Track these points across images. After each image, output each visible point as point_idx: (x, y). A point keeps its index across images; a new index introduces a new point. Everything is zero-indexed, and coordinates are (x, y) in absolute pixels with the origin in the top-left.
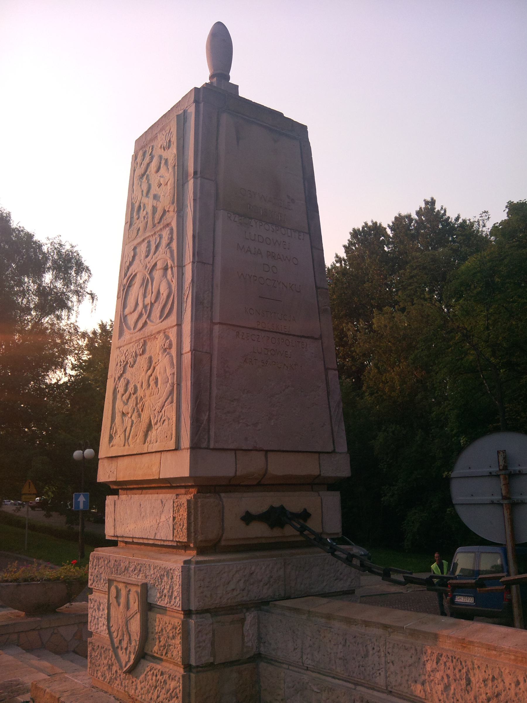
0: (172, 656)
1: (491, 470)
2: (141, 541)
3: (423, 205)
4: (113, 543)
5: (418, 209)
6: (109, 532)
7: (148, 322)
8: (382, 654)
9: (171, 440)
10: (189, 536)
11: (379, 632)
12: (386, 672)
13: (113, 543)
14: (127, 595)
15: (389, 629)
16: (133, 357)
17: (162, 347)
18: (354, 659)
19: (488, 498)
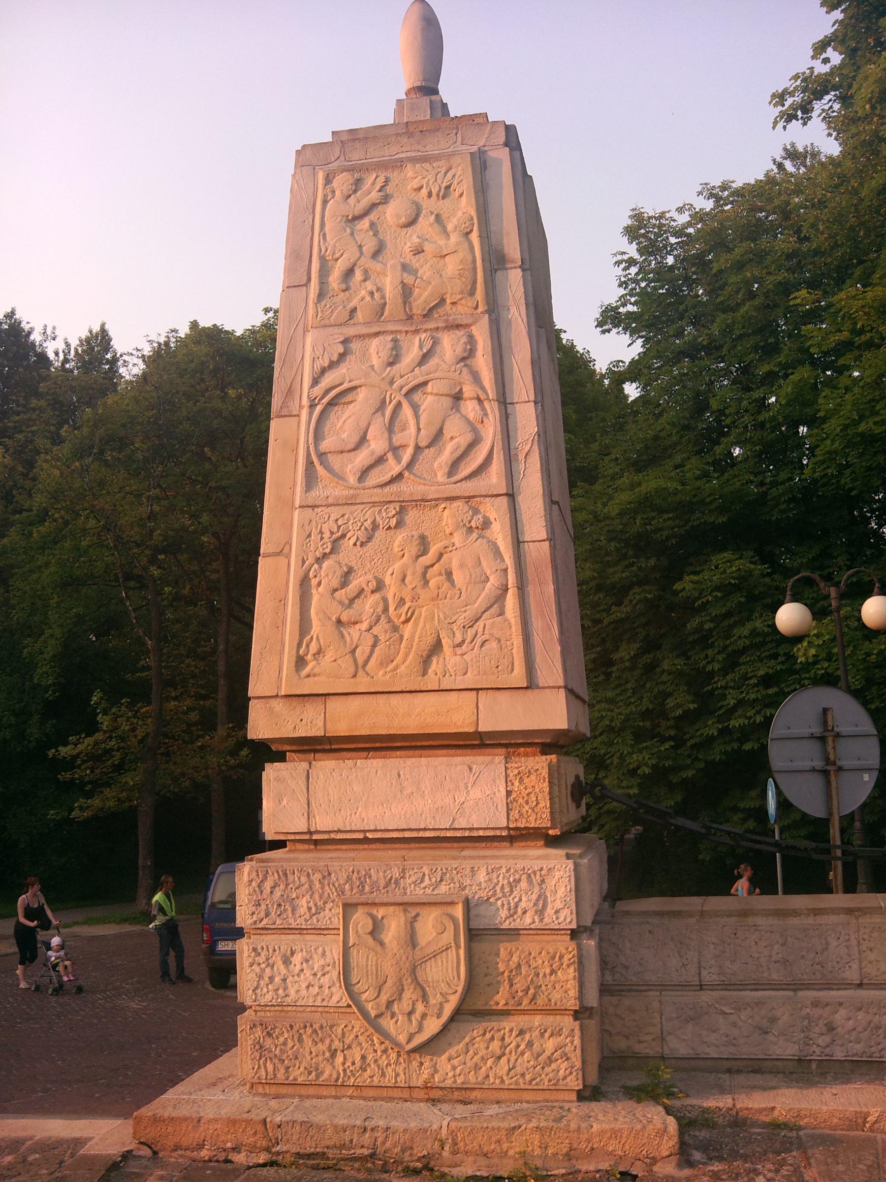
0: (550, 1000)
1: (810, 731)
2: (395, 835)
3: (184, 331)
4: (279, 845)
5: (9, 311)
6: (270, 829)
7: (406, 474)
8: (854, 943)
9: (512, 670)
10: (553, 819)
11: (842, 918)
12: (860, 961)
13: (279, 845)
14: (408, 925)
15: (856, 913)
16: (366, 529)
17: (464, 525)
18: (803, 957)
19: (808, 764)
